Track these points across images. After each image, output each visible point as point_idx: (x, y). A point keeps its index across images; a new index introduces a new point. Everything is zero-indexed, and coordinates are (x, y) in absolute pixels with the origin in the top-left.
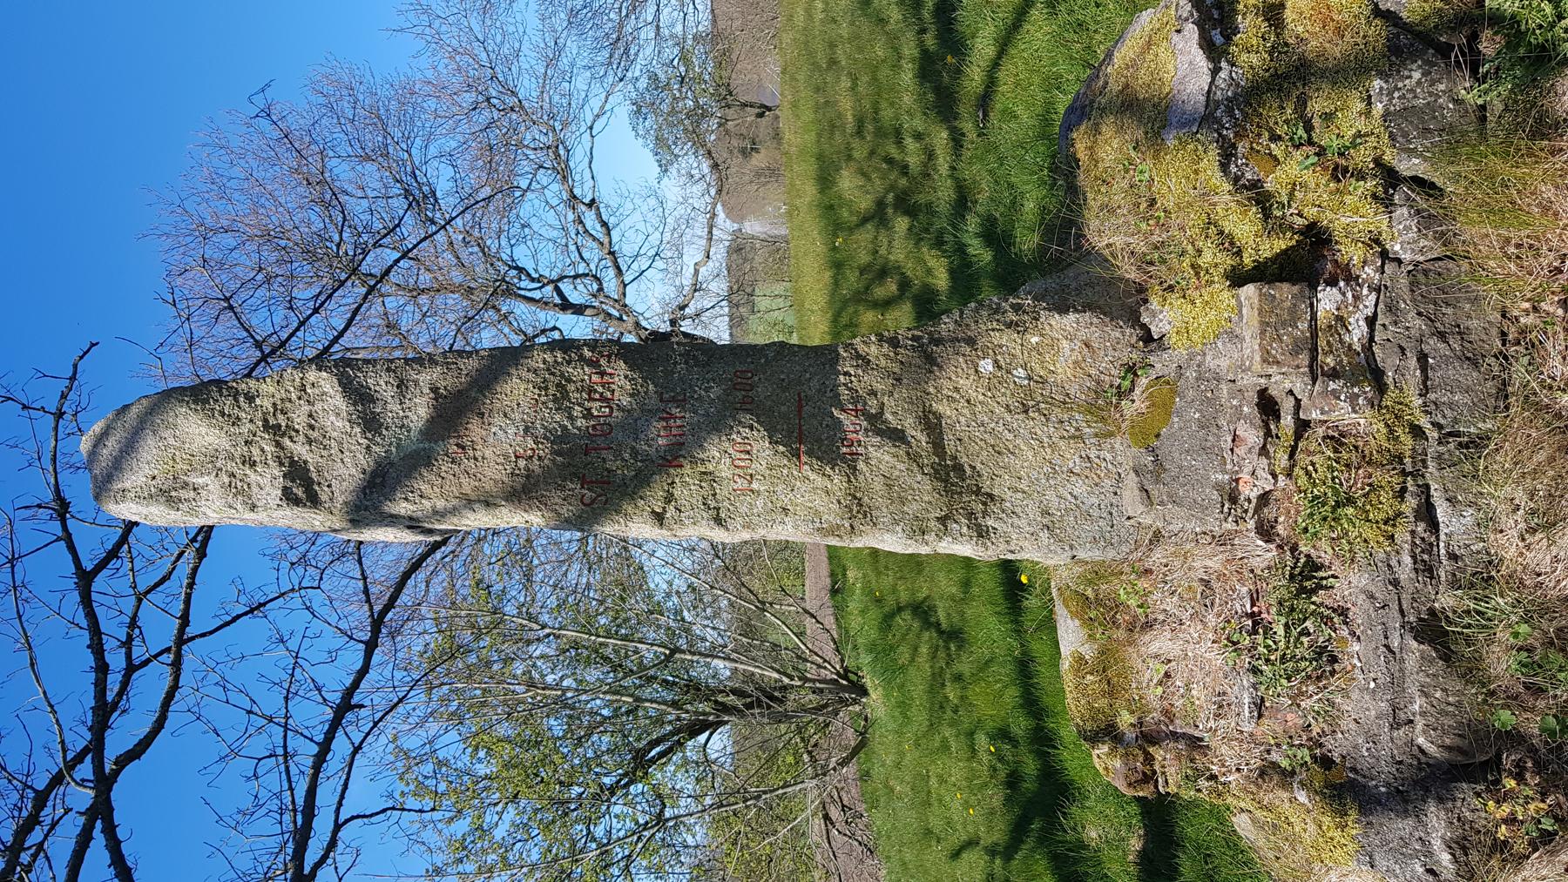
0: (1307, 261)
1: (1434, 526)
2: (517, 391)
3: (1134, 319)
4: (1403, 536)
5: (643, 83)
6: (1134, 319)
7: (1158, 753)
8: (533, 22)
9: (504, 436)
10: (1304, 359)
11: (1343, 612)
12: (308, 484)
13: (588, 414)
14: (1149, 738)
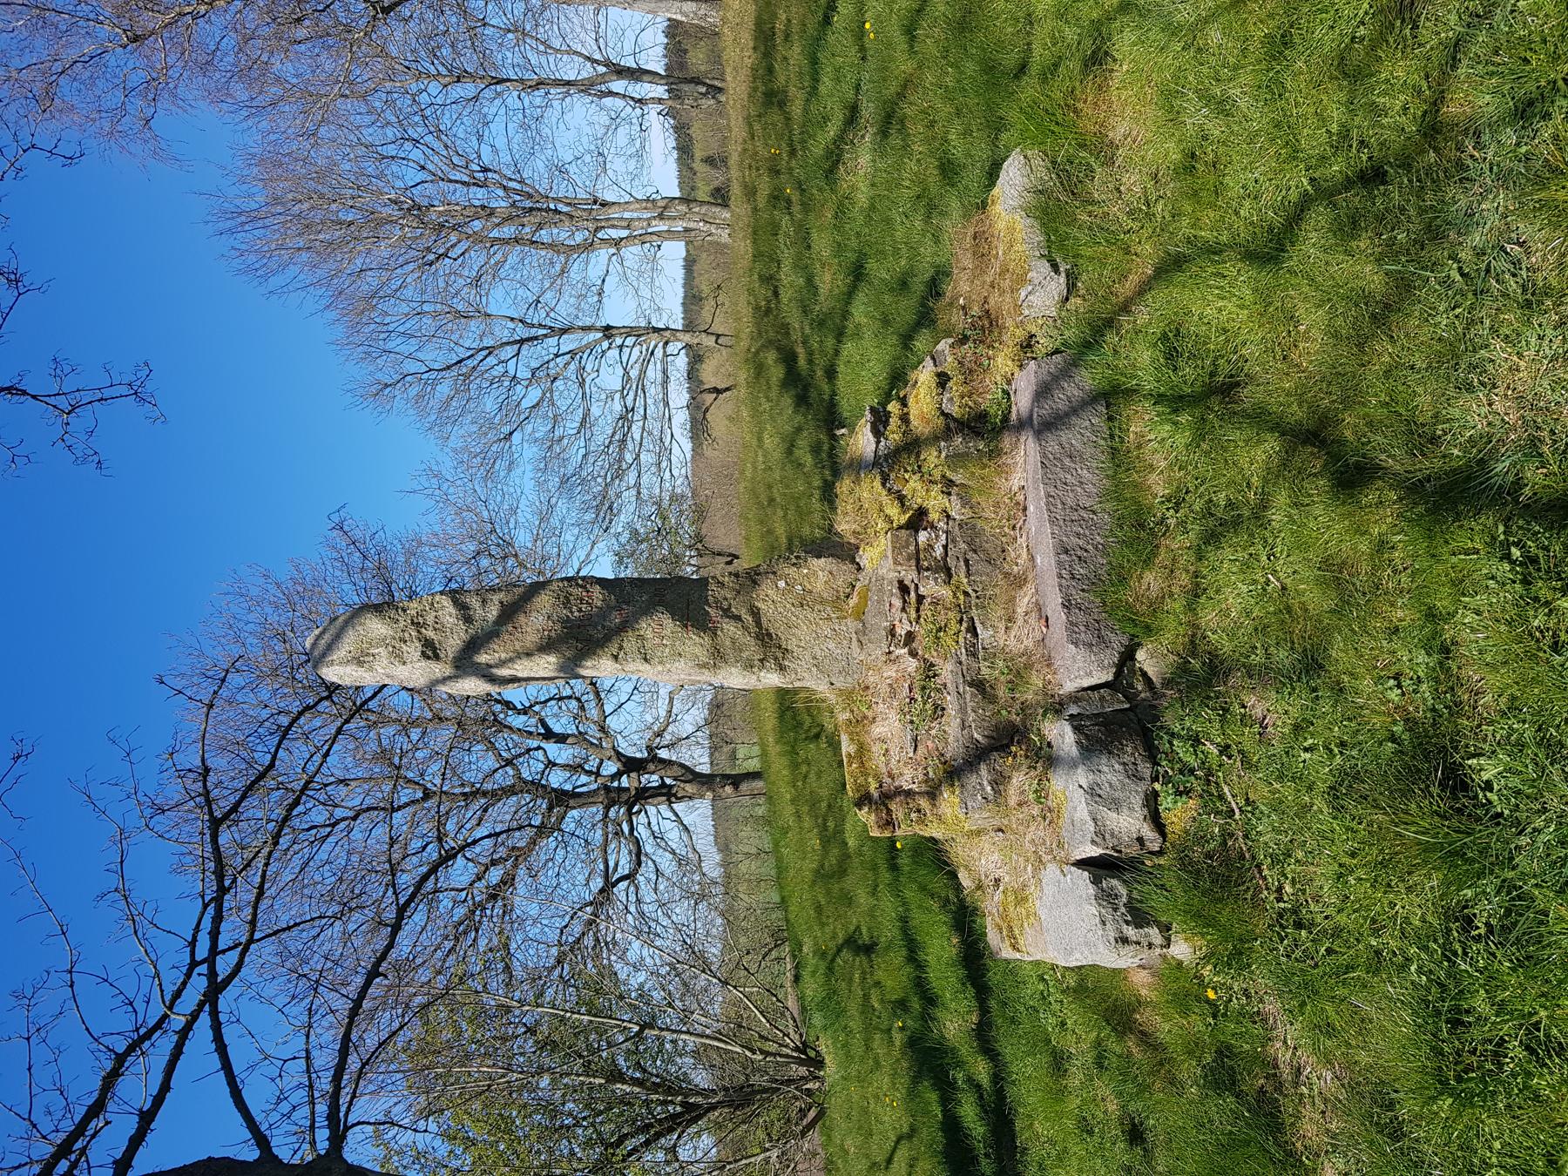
0: (918, 520)
1: (976, 635)
2: (544, 601)
3: (853, 561)
4: (961, 640)
5: (626, 535)
6: (853, 561)
7: (893, 807)
8: (529, 485)
9: (538, 620)
10: (913, 562)
11: (945, 685)
12: (434, 649)
13: (580, 610)
14: (886, 797)
